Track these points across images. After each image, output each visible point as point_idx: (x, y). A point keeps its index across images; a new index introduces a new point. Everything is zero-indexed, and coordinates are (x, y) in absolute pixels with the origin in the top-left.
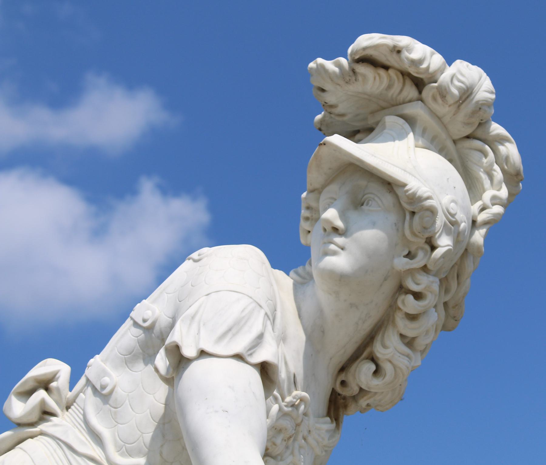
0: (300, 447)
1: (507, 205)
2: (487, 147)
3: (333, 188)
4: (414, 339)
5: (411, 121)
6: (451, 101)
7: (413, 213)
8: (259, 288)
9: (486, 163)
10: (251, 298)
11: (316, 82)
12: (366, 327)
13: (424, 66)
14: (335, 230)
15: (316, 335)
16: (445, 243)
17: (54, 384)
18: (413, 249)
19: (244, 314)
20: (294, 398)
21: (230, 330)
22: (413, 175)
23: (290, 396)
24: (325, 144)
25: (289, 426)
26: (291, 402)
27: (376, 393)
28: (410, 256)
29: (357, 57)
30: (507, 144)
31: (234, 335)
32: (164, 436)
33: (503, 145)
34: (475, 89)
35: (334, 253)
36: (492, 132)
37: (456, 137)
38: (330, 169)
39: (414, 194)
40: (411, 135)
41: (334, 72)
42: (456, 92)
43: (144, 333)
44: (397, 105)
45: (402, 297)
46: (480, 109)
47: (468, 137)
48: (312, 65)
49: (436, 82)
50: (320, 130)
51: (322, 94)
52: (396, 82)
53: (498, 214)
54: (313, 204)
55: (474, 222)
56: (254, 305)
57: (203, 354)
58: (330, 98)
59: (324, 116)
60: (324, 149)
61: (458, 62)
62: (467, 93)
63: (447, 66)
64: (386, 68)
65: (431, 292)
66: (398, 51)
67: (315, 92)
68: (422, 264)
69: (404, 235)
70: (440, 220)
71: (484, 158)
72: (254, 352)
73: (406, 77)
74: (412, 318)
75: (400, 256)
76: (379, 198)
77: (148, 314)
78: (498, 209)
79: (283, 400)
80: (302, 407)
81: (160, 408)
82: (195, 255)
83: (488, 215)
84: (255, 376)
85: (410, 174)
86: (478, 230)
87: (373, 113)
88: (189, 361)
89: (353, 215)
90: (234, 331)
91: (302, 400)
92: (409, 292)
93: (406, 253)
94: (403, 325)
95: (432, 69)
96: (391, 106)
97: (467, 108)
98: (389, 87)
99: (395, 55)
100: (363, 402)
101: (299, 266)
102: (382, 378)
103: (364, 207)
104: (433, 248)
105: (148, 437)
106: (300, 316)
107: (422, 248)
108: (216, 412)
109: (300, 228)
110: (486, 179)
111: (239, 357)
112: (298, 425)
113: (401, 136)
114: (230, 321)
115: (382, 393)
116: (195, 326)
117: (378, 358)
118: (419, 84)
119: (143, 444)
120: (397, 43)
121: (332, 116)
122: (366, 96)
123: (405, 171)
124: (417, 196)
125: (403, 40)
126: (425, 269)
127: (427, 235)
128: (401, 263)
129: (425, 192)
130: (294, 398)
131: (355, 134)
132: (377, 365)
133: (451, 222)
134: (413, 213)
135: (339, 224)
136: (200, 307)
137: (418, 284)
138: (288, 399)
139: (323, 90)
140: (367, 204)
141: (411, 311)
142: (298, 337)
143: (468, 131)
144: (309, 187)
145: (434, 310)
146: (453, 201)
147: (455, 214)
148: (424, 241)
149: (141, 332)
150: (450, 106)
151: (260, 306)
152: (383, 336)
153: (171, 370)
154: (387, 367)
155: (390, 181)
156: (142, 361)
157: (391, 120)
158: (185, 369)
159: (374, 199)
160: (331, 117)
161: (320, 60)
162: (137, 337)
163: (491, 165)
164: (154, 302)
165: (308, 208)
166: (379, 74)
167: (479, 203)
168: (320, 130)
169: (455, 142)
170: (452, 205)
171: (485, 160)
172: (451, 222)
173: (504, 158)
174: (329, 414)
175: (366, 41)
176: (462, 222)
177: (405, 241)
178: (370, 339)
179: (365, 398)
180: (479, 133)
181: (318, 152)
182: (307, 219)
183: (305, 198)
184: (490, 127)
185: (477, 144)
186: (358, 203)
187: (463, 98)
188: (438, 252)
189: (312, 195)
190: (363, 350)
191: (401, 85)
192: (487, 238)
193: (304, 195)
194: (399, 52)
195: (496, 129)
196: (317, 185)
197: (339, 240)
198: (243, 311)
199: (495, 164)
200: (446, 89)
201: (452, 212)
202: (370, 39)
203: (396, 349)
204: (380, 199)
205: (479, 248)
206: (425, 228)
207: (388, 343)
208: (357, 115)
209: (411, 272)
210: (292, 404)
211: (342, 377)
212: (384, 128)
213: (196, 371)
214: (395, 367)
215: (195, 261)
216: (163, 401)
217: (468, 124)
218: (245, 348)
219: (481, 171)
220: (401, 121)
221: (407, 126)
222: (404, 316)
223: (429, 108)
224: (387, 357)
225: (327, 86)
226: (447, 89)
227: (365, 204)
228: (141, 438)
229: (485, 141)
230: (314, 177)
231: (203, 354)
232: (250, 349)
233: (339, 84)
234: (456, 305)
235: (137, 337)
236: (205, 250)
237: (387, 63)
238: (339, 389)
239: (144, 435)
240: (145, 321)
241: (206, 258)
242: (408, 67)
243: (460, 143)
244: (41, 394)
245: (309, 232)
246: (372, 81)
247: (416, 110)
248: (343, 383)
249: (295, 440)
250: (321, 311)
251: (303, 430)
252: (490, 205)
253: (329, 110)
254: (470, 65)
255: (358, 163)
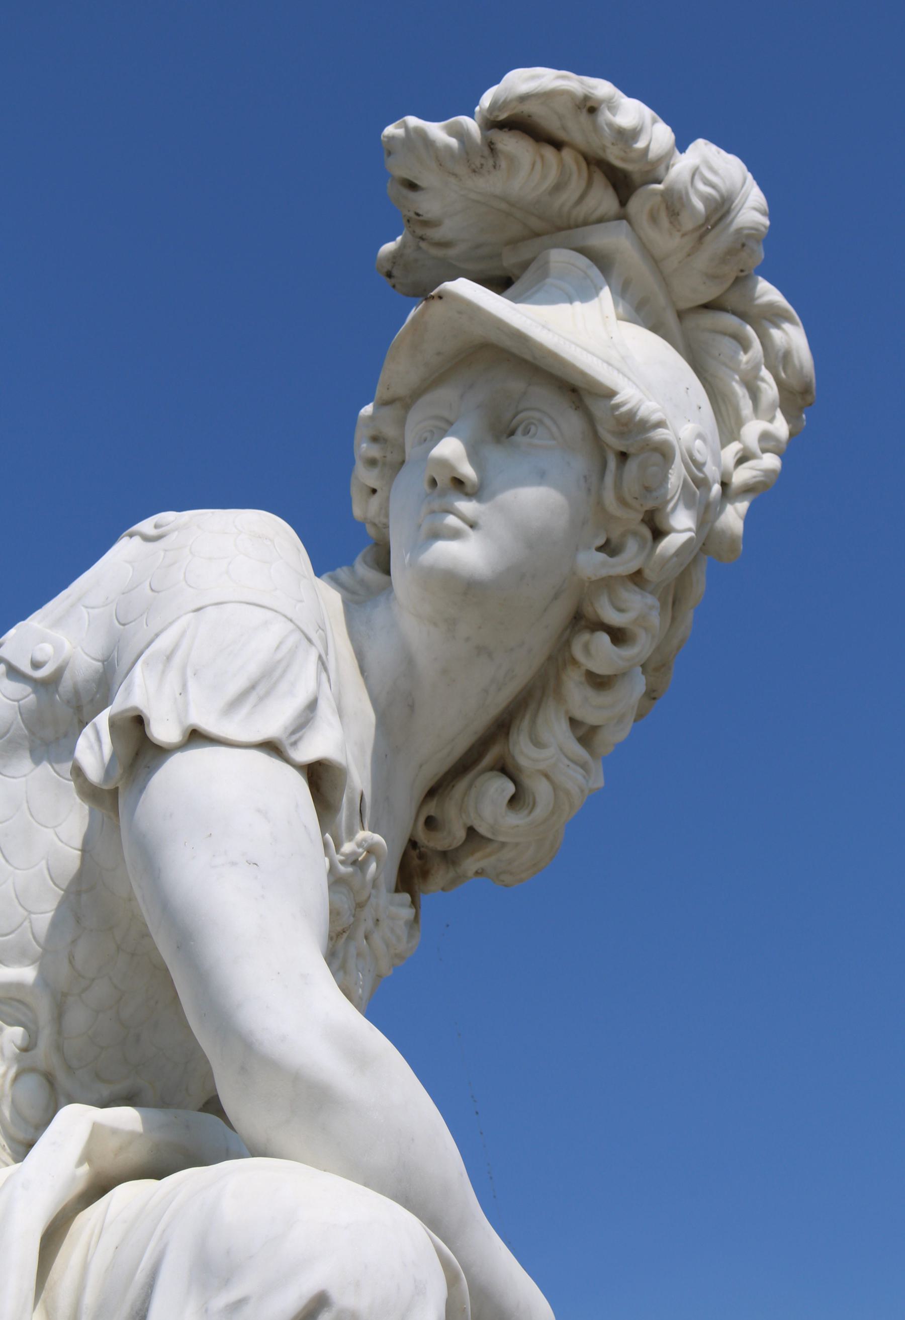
0: (359, 955)
1: (789, 452)
2: (749, 329)
3: (446, 395)
4: (594, 729)
5: (603, 262)
6: (688, 223)
7: (623, 456)
8: (301, 601)
9: (747, 363)
10: (291, 620)
11: (399, 168)
13: (640, 145)
14: (458, 483)
15: (396, 711)
16: (682, 524)
18: (615, 535)
19: (279, 655)
20: (359, 845)
21: (252, 687)
22: (625, 375)
23: (350, 840)
24: (440, 297)
25: (346, 906)
26: (354, 853)
27: (503, 845)
28: (609, 548)
29: (503, 116)
30: (786, 326)
31: (261, 699)
32: (78, 920)
33: (778, 327)
34: (737, 202)
35: (455, 534)
36: (759, 297)
37: (684, 305)
38: (439, 354)
39: (632, 414)
40: (606, 293)
41: (448, 148)
43: (35, 691)
44: (569, 227)
45: (585, 637)
46: (743, 245)
47: (708, 306)
48: (391, 130)
49: (659, 182)
50: (389, 275)
51: (412, 195)
52: (575, 177)
53: (773, 471)
54: (390, 431)
56: (296, 637)
57: (196, 737)
58: (428, 205)
59: (403, 245)
60: (437, 307)
61: (700, 142)
62: (721, 208)
63: (677, 152)
65: (646, 629)
66: (590, 107)
67: (393, 190)
68: (633, 567)
69: (600, 504)
70: (676, 476)
71: (742, 353)
72: (300, 738)
73: (594, 168)
74: (600, 682)
75: (589, 548)
76: (552, 419)
77: (45, 651)
78: (771, 461)
79: (338, 846)
80: (373, 867)
81: (72, 858)
82: (146, 526)
83: (755, 473)
84: (298, 788)
85: (619, 371)
86: (732, 503)
87: (513, 243)
88: (161, 752)
89: (495, 455)
90: (261, 690)
91: (371, 850)
92: (601, 626)
93: (601, 541)
94: (578, 698)
95: (653, 153)
96: (560, 228)
97: (717, 243)
98: (558, 187)
99: (584, 117)
100: (471, 864)
101: (340, 566)
102: (526, 812)
103: (518, 438)
104: (658, 534)
105: (43, 920)
106: (363, 670)
107: (635, 534)
108: (234, 864)
109: (353, 481)
110: (744, 396)
111: (271, 747)
112: (360, 906)
113: (586, 294)
114: (253, 669)
115: (517, 844)
116: (173, 677)
117: (518, 768)
118: (623, 184)
119: (31, 936)
120: (592, 91)
121: (423, 245)
122: (503, 206)
123: (609, 364)
124: (638, 418)
125: (602, 88)
126: (637, 578)
127: (649, 505)
128: (592, 563)
129: (654, 411)
130: (359, 845)
131: (501, 283)
133: (695, 480)
134: (623, 456)
135: (468, 471)
136: (183, 634)
137: (621, 610)
138: (348, 847)
139: (412, 186)
140: (526, 432)
141: (601, 668)
142: (365, 714)
143: (710, 293)
144: (380, 392)
145: (640, 669)
146: (700, 436)
147: (704, 464)
148: (640, 517)
149: (28, 689)
150: (683, 235)
151: (309, 640)
152: (533, 721)
153: (118, 771)
154: (541, 789)
155: (578, 382)
156: (28, 754)
157: (560, 258)
159: (541, 422)
160: (419, 248)
161: (413, 121)
162: (18, 701)
163: (757, 368)
164: (57, 623)
165: (375, 439)
166: (542, 157)
167: (734, 448)
168: (389, 275)
169: (681, 315)
170: (698, 443)
171: (744, 358)
172: (695, 480)
173: (781, 354)
175: (524, 81)
176: (714, 482)
178: (502, 727)
179: (478, 855)
180: (733, 300)
181: (422, 314)
182: (372, 462)
183: (372, 418)
184: (755, 286)
185: (730, 321)
186: (501, 431)
187: (713, 221)
188: (672, 543)
189: (386, 411)
190: (488, 750)
191: (583, 184)
192: (749, 519)
193: (367, 410)
195: (767, 292)
196: (400, 390)
197: (466, 506)
198: (278, 648)
199: (763, 367)
200: (681, 198)
201: (698, 457)
202: (533, 78)
203: (561, 750)
204: (555, 422)
205: (733, 540)
206: (648, 489)
208: (478, 246)
209: (607, 584)
210: (353, 858)
211: (431, 809)
212: (544, 273)
214: (555, 787)
215: (147, 539)
216: (78, 842)
217: (713, 277)
218: (286, 728)
219: (734, 379)
220: (583, 261)
221: (595, 272)
222: (583, 679)
223: (640, 238)
224: (542, 766)
225: (424, 179)
226: (684, 197)
227: (520, 431)
228: (27, 924)
229: (744, 316)
230: (398, 371)
231: (196, 737)
232: (293, 732)
233: (455, 175)
234: (663, 665)
235: (18, 701)
236: (168, 517)
237: (561, 135)
238: (422, 836)
239: (33, 916)
240: (36, 665)
241: (176, 533)
242: (608, 144)
243: (696, 320)
245: (374, 491)
246: (527, 172)
247: (615, 239)
249: (349, 938)
250: (409, 662)
252: (759, 452)
253: (420, 231)
254: (723, 152)
255: (507, 343)
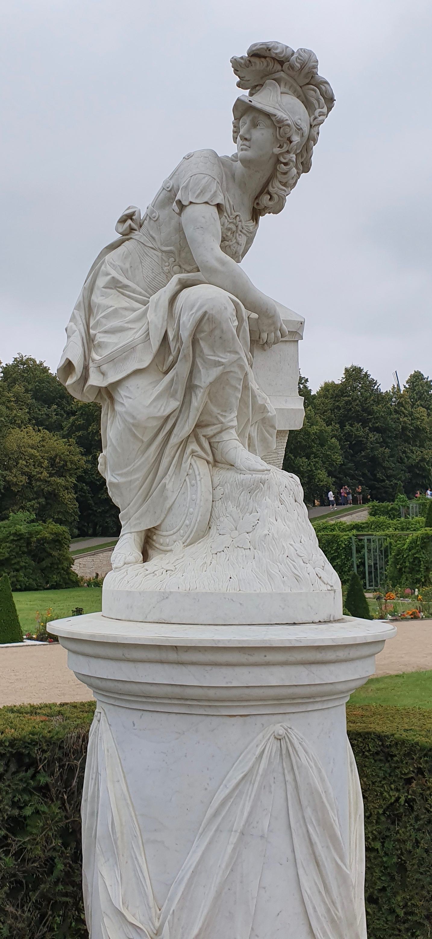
0: (239, 235)
5: (278, 81)
7: (280, 128)
12: (264, 180)
17: (134, 217)
28: (281, 147)
42: (299, 65)
49: (289, 61)
55: (311, 125)
57: (191, 203)
64: (265, 57)
68: (286, 150)
69: (319, 89)
84: (215, 209)
92: (282, 163)
98: (268, 65)
104: (291, 142)
107: (286, 143)
111: (206, 203)
132: (271, 196)
143: (307, 81)
154: (275, 196)
158: (184, 209)
170: (299, 121)
174: (252, 219)
177: (277, 140)
180: (312, 82)
186: (254, 125)
188: (294, 143)
194: (270, 50)
207: (274, 186)
209: (282, 154)
211: (257, 201)
213: (189, 210)
214: (279, 196)
238: (255, 206)
244: (129, 222)
248: (258, 204)
251: (240, 227)
